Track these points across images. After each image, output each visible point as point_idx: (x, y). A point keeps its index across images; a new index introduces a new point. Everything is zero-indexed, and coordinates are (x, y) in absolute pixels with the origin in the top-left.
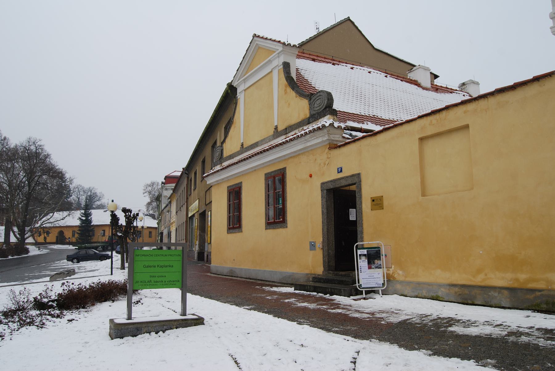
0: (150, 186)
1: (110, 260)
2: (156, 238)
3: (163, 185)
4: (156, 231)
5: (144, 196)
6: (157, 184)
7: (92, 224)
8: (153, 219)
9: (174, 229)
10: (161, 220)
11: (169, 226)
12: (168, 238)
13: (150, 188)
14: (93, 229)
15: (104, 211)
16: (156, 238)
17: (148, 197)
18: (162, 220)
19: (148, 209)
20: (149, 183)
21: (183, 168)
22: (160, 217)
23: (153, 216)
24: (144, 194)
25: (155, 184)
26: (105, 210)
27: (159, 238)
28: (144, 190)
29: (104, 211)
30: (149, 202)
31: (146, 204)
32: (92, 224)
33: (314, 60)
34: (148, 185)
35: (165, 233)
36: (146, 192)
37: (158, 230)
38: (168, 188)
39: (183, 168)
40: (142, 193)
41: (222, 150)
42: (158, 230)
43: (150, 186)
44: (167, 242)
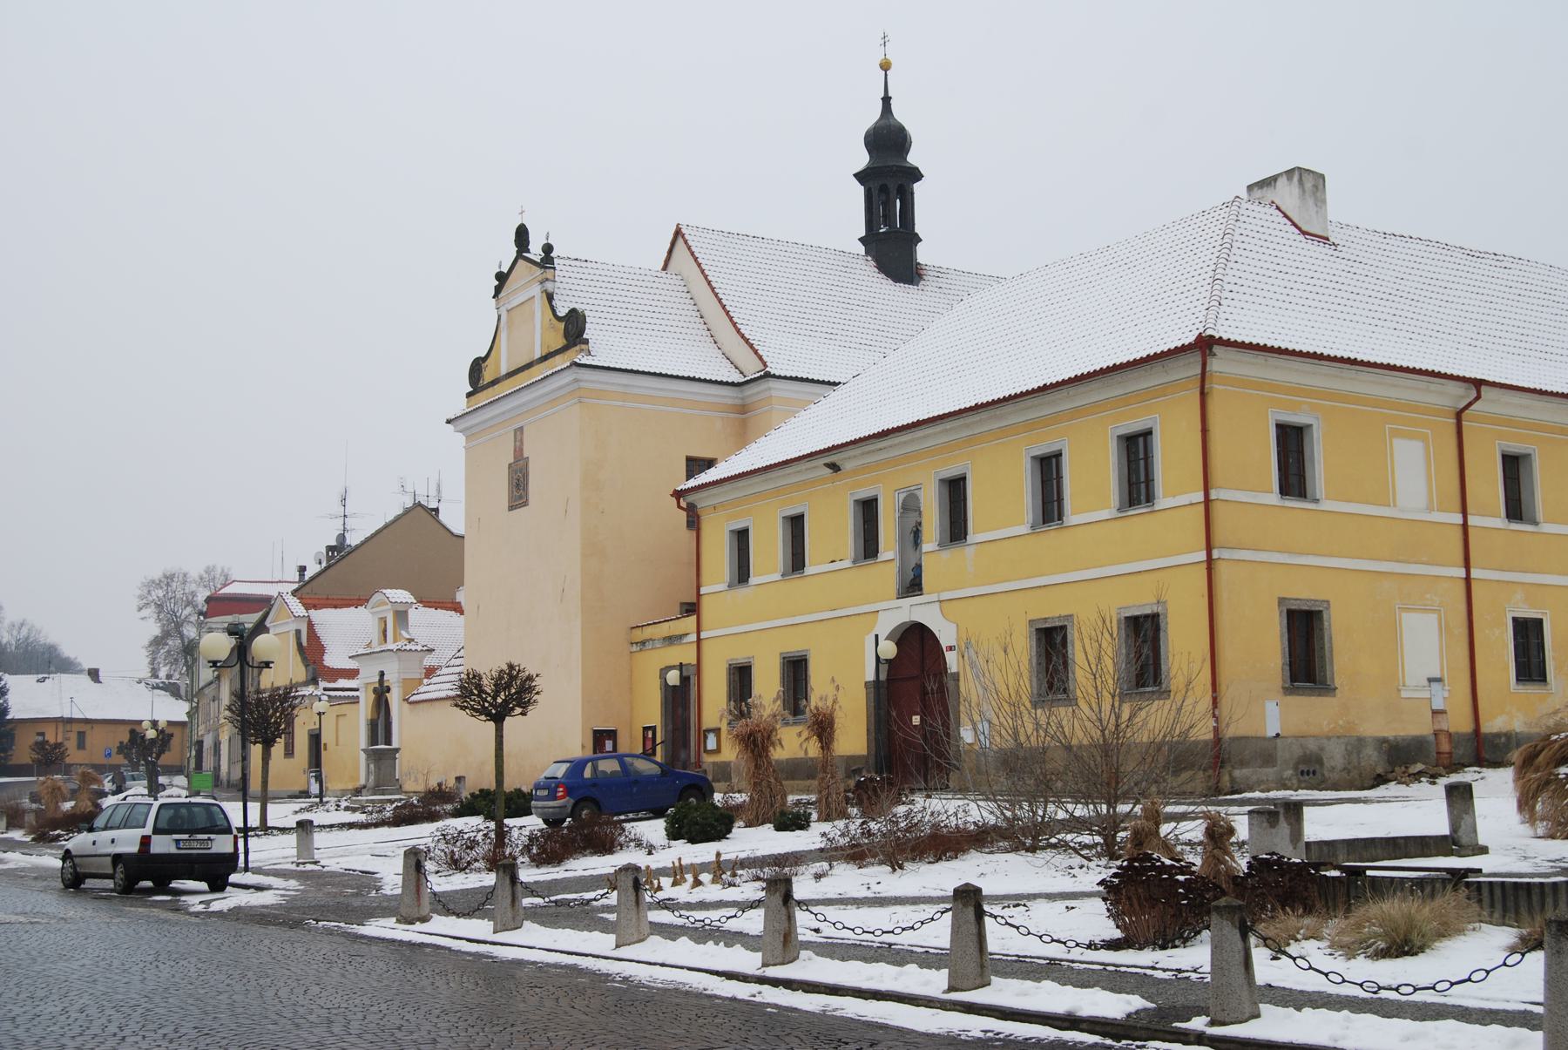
0: (161, 588)
1: (694, 618)
2: (182, 753)
3: (202, 618)
4: (183, 733)
5: (142, 619)
6: (181, 578)
7: (8, 717)
8: (173, 699)
9: (227, 737)
10: (197, 707)
11: (217, 730)
12: (215, 755)
13: (161, 593)
14: (11, 729)
15: (38, 681)
16: (182, 753)
17: (152, 620)
18: (200, 710)
19: (154, 659)
20: (157, 574)
21: (916, 175)
22: (196, 700)
23: (173, 690)
24: (140, 609)
25: (175, 579)
26: (40, 676)
27: (194, 753)
28: (141, 597)
29: (38, 681)
30: (157, 637)
31: (146, 643)
32: (8, 717)
33: (336, 607)
34: (153, 582)
35: (208, 742)
36: (147, 605)
37: (188, 730)
38: (214, 626)
39: (916, 175)
40: (135, 608)
41: (259, 682)
42: (188, 730)
43: (158, 585)
44: (1404, 694)
